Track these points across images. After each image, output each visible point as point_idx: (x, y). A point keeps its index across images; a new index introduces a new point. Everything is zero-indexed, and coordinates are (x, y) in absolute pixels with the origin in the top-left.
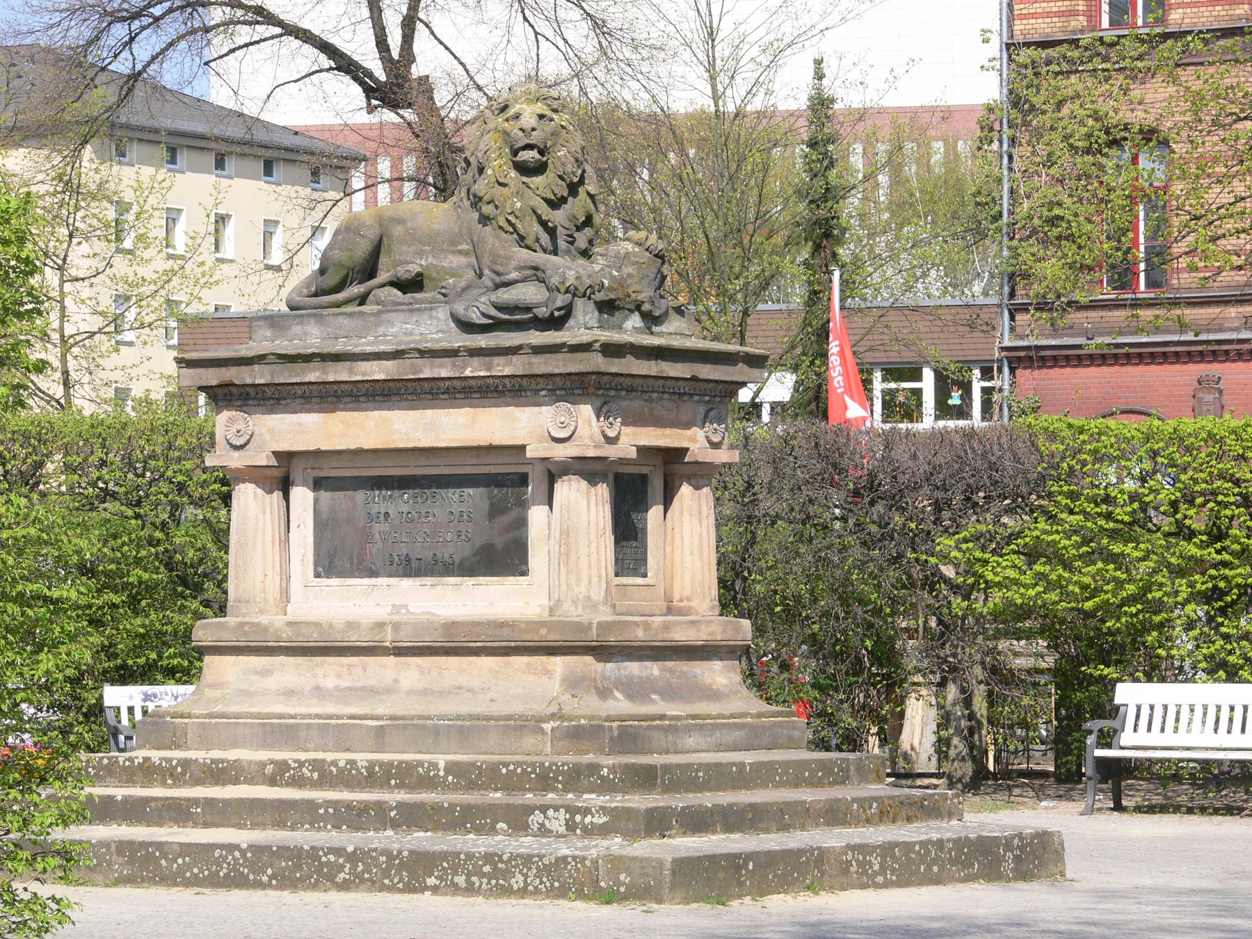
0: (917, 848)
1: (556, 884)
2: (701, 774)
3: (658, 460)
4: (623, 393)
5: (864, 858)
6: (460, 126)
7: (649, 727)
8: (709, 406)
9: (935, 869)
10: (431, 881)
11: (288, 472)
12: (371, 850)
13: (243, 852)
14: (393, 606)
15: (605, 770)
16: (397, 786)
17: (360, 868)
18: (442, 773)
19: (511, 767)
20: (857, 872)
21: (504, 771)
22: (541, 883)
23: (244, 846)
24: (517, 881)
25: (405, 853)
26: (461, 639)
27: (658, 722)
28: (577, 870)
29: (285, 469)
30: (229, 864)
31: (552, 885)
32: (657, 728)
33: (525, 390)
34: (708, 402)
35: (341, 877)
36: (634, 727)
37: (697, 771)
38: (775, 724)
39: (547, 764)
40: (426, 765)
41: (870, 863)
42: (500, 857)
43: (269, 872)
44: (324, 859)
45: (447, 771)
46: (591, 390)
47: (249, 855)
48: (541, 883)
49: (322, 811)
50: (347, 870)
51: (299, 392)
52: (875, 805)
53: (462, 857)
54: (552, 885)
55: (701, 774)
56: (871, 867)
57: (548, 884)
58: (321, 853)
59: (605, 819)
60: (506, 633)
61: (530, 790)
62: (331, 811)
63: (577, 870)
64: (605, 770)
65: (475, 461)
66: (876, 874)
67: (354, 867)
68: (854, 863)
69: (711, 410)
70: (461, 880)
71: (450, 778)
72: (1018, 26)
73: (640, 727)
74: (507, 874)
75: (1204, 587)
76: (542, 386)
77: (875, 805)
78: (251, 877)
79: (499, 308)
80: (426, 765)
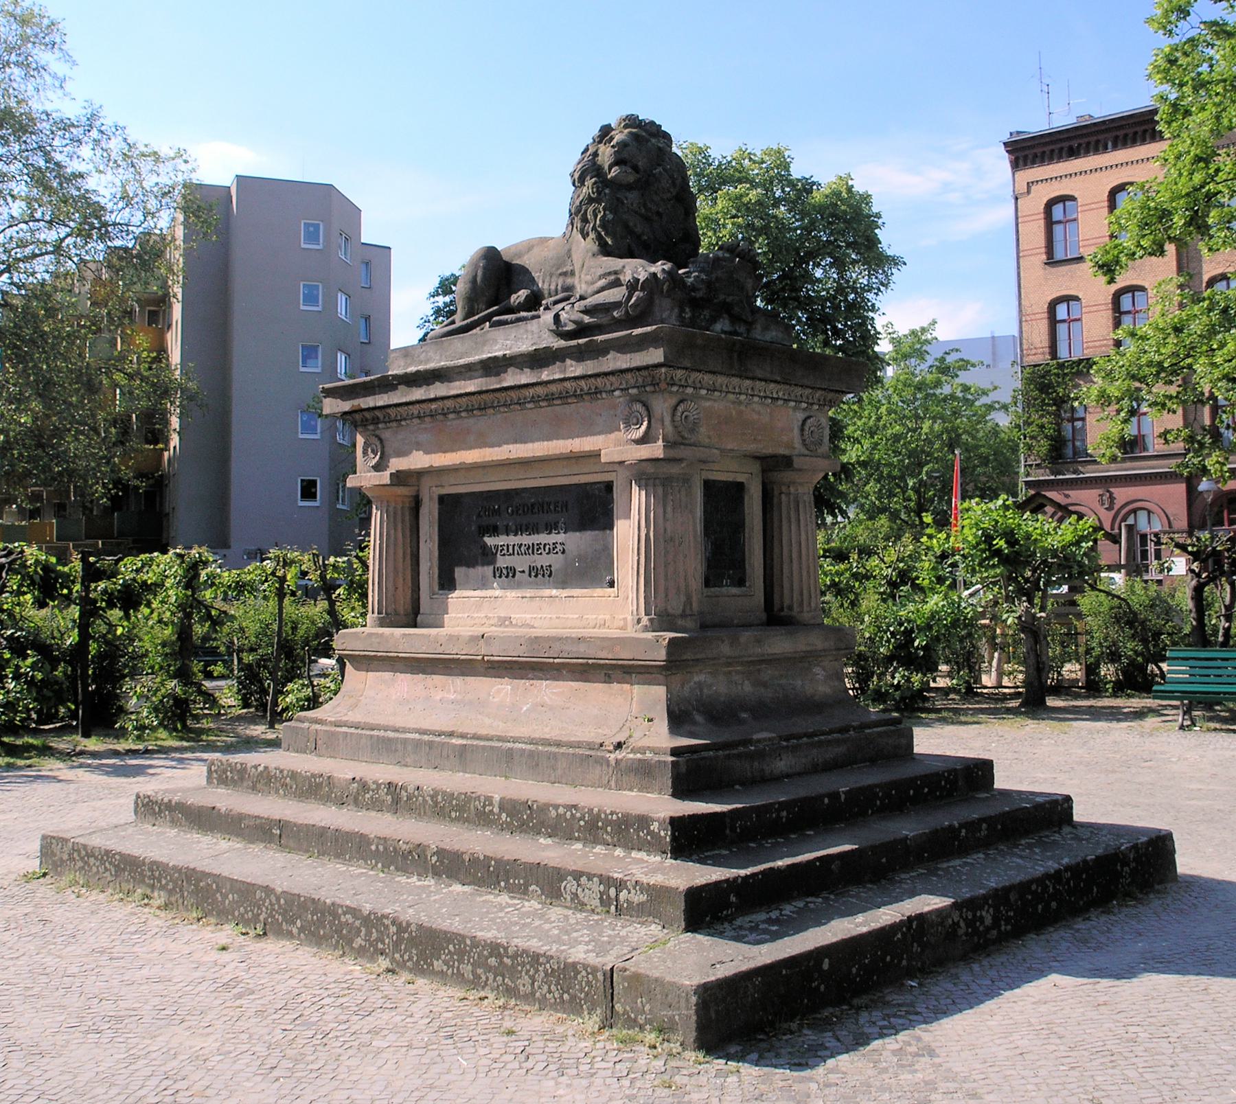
0: (1034, 887)
1: (566, 996)
2: (784, 814)
3: (756, 467)
4: (704, 392)
5: (974, 915)
6: (1024, 662)
7: (728, 757)
8: (807, 414)
9: (1054, 905)
10: (438, 965)
11: (418, 491)
12: (384, 916)
13: (278, 899)
14: (499, 618)
15: (656, 824)
16: (457, 819)
17: (375, 935)
18: (496, 810)
19: (561, 810)
20: (966, 934)
21: (553, 813)
22: (550, 992)
23: (279, 890)
24: (524, 984)
25: (413, 927)
26: (543, 656)
27: (741, 749)
28: (589, 983)
29: (416, 488)
30: (267, 909)
31: (561, 997)
32: (739, 756)
33: (601, 392)
34: (804, 409)
35: (359, 942)
36: (710, 758)
37: (778, 811)
38: (880, 734)
39: (596, 810)
40: (482, 799)
41: (982, 919)
42: (506, 949)
43: (299, 923)
44: (343, 919)
45: (502, 808)
46: (663, 385)
47: (282, 901)
48: (550, 992)
49: (373, 847)
50: (363, 933)
51: (416, 412)
52: (984, 826)
53: (468, 942)
54: (561, 997)
55: (784, 814)
56: (982, 922)
57: (557, 995)
58: (340, 911)
59: (643, 898)
60: (582, 649)
61: (578, 839)
62: (381, 848)
63: (589, 983)
64: (656, 824)
65: (566, 471)
66: (988, 929)
67: (369, 933)
68: (962, 924)
69: (809, 417)
70: (467, 969)
71: (504, 816)
72: (1025, 359)
73: (717, 757)
74: (513, 972)
75: (337, 592)
76: (616, 385)
77: (984, 826)
78: (284, 926)
79: (586, 312)
80: (482, 799)
